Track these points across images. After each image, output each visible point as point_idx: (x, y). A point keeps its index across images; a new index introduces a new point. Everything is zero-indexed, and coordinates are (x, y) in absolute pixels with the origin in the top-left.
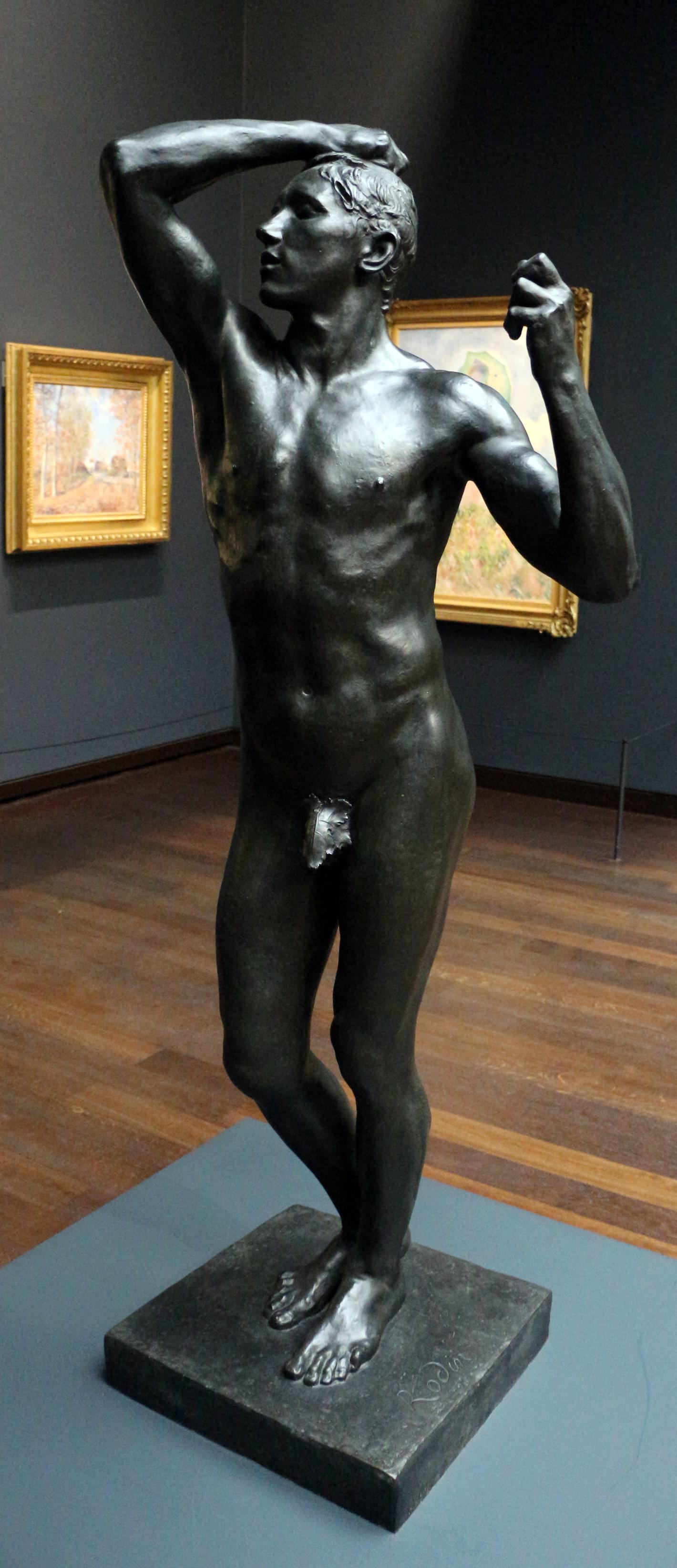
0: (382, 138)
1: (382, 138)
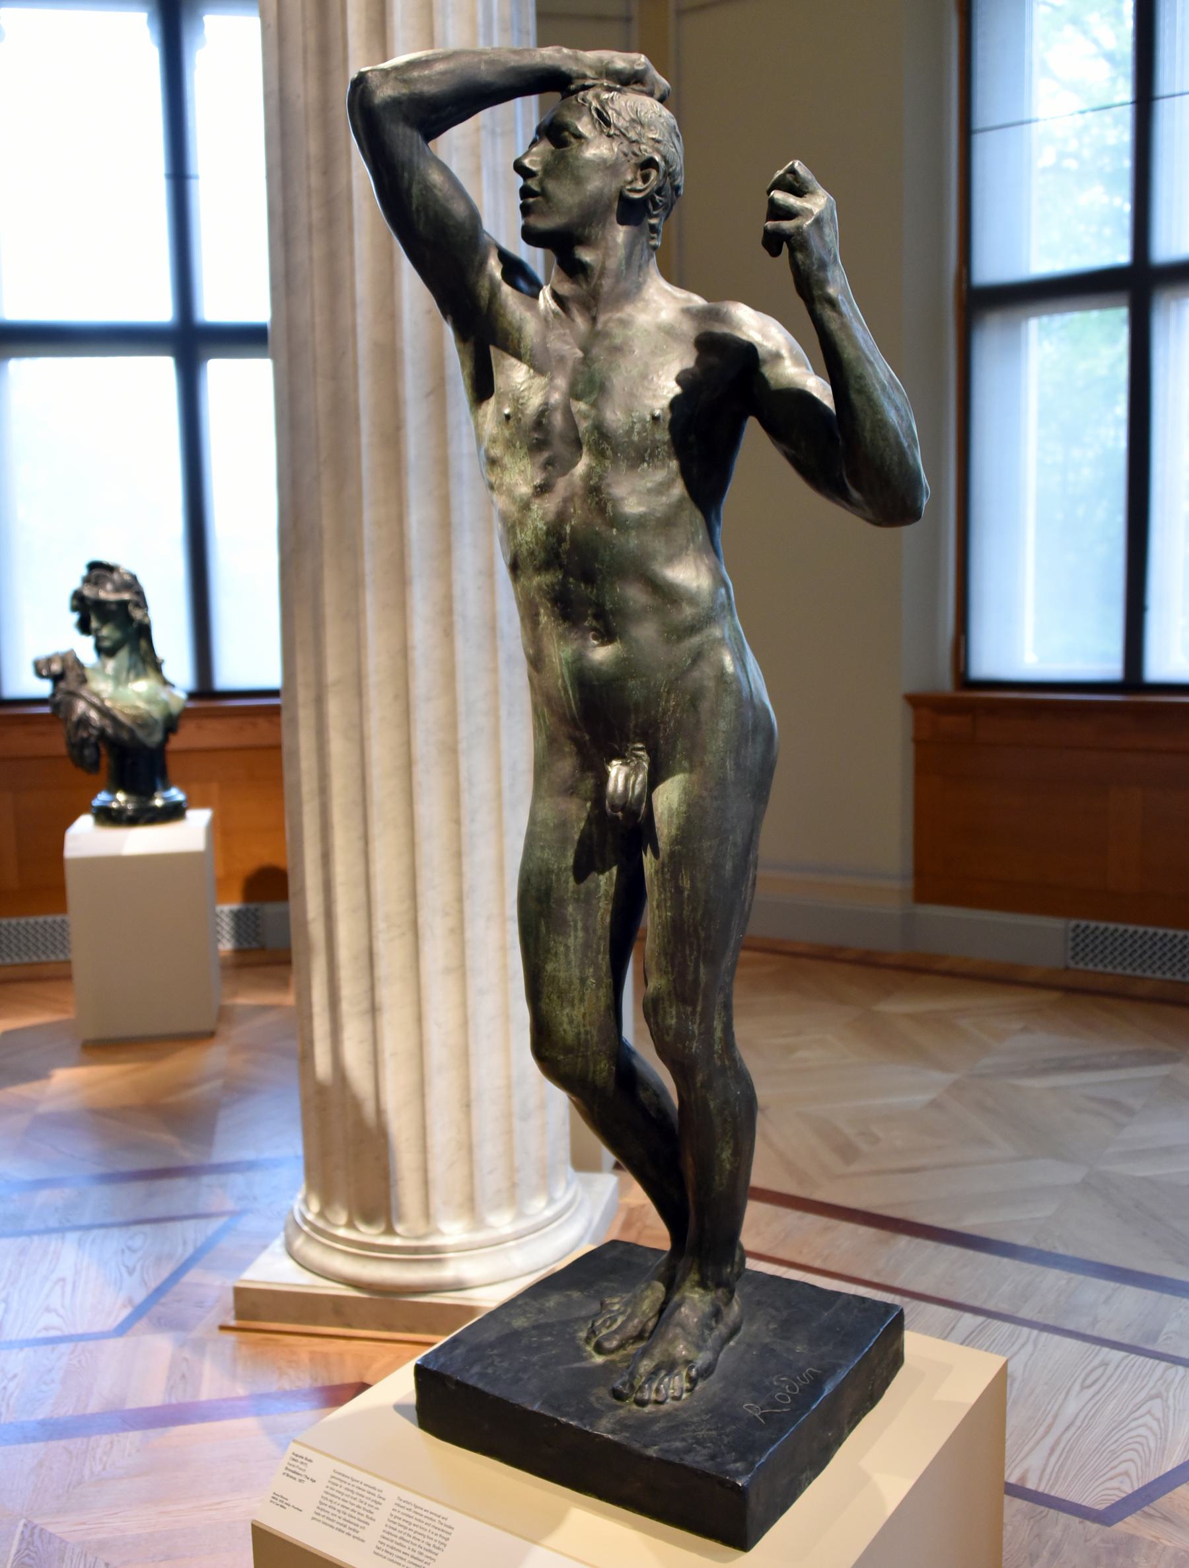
0: (640, 60)
1: (640, 60)
